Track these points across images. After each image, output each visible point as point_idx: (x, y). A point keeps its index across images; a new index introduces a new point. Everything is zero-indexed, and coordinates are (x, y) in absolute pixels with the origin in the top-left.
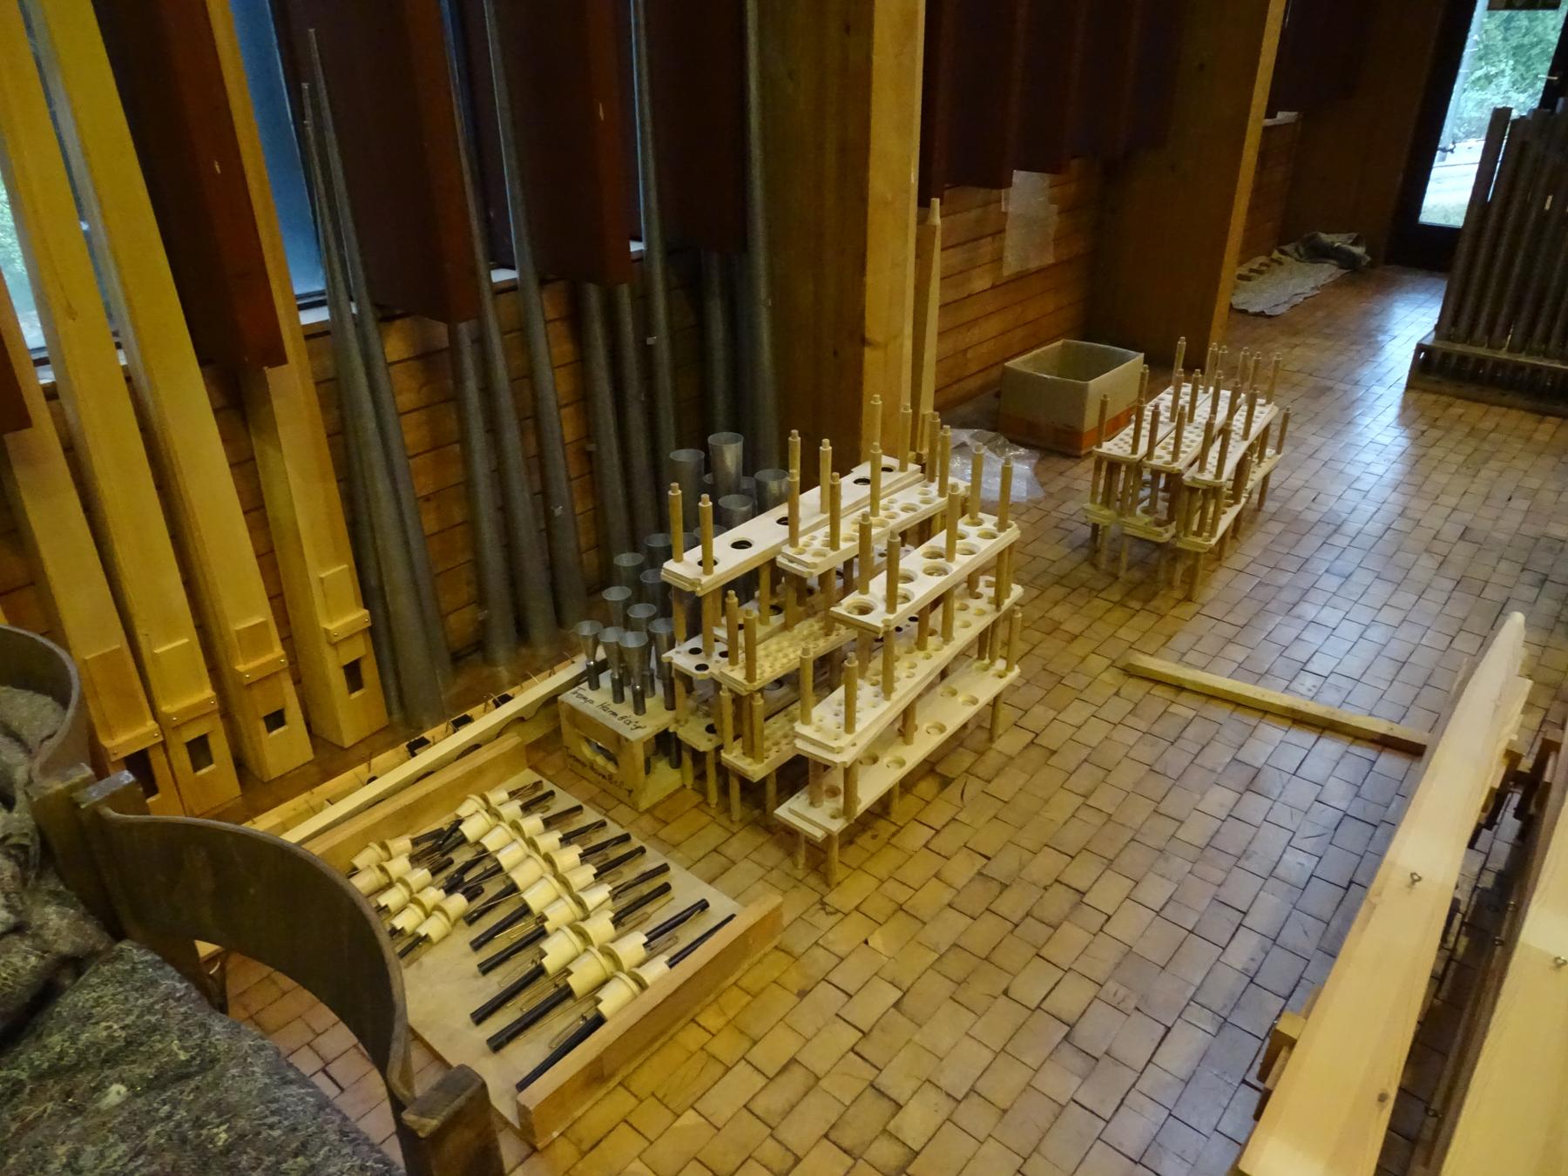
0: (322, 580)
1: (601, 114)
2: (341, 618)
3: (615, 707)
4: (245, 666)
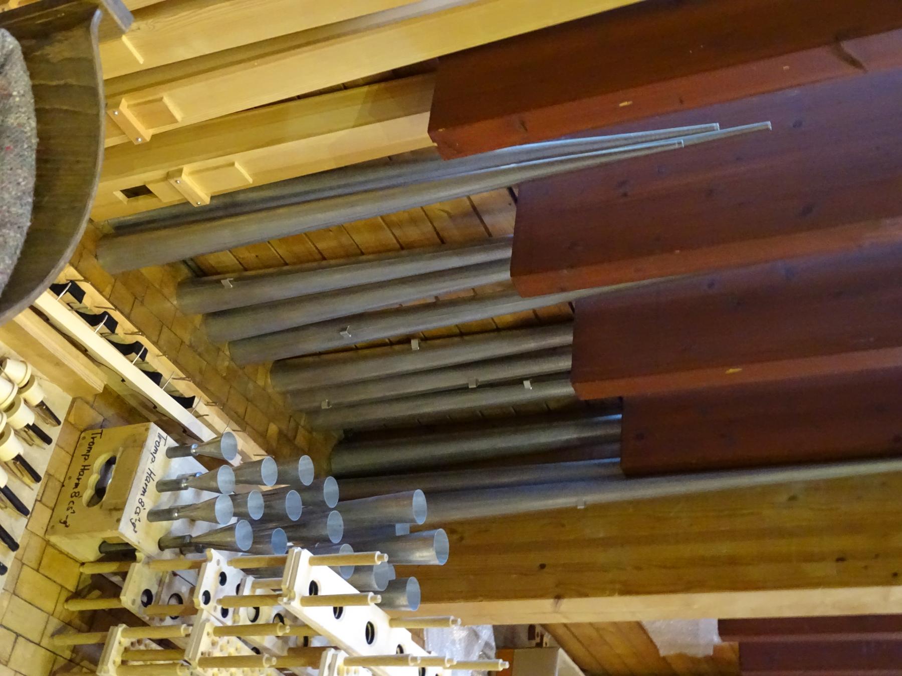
0: (233, 164)
1: (731, 371)
3: (152, 486)
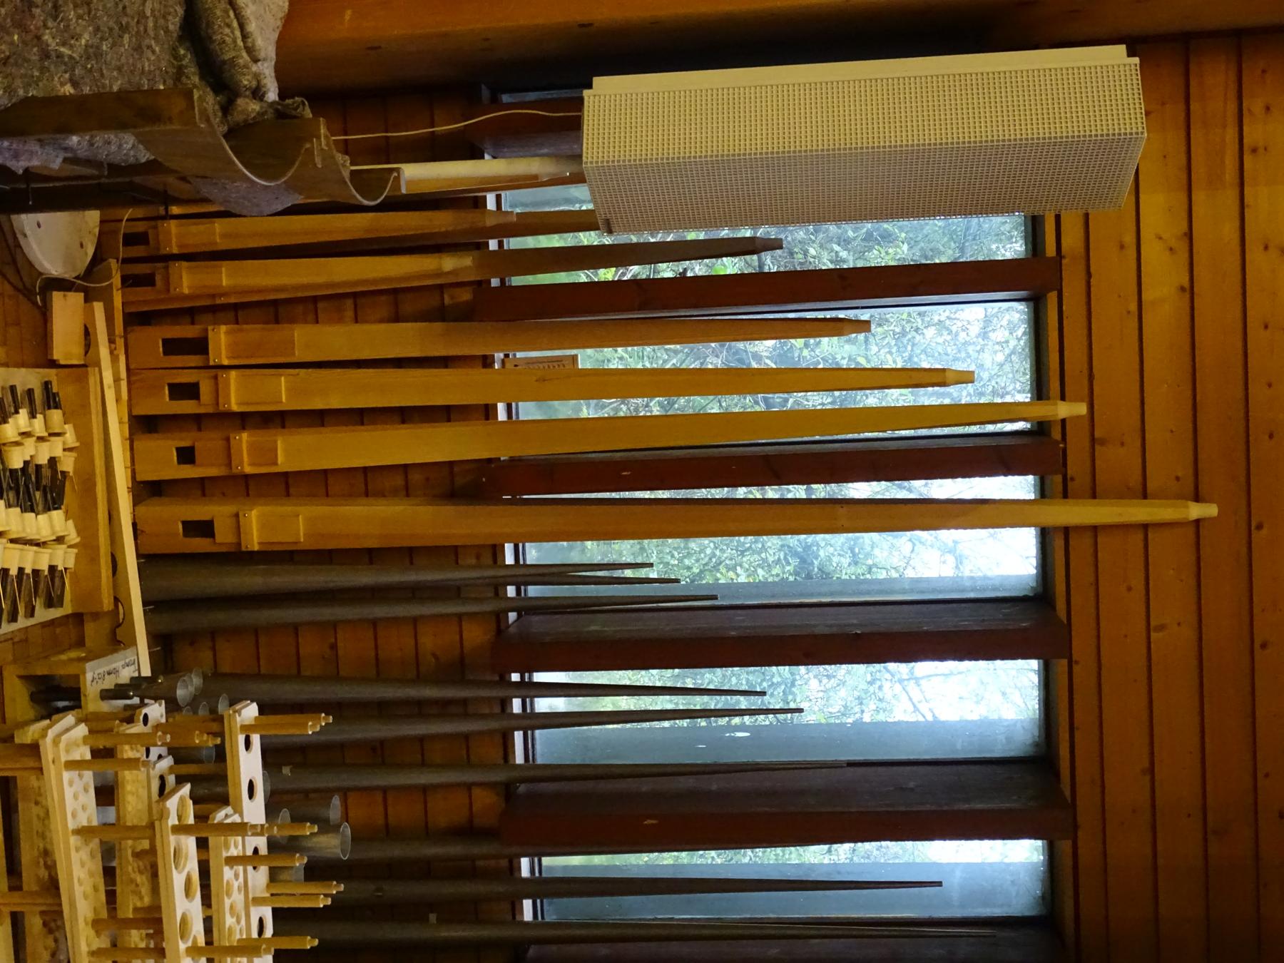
2: (258, 524)
4: (244, 440)
